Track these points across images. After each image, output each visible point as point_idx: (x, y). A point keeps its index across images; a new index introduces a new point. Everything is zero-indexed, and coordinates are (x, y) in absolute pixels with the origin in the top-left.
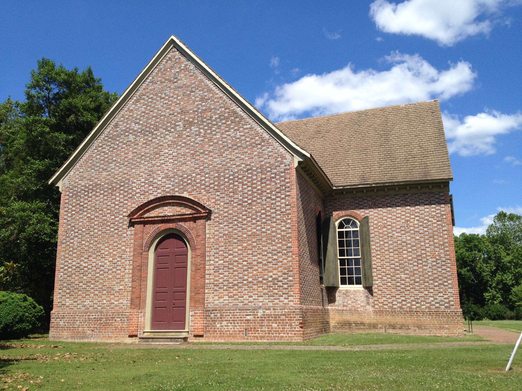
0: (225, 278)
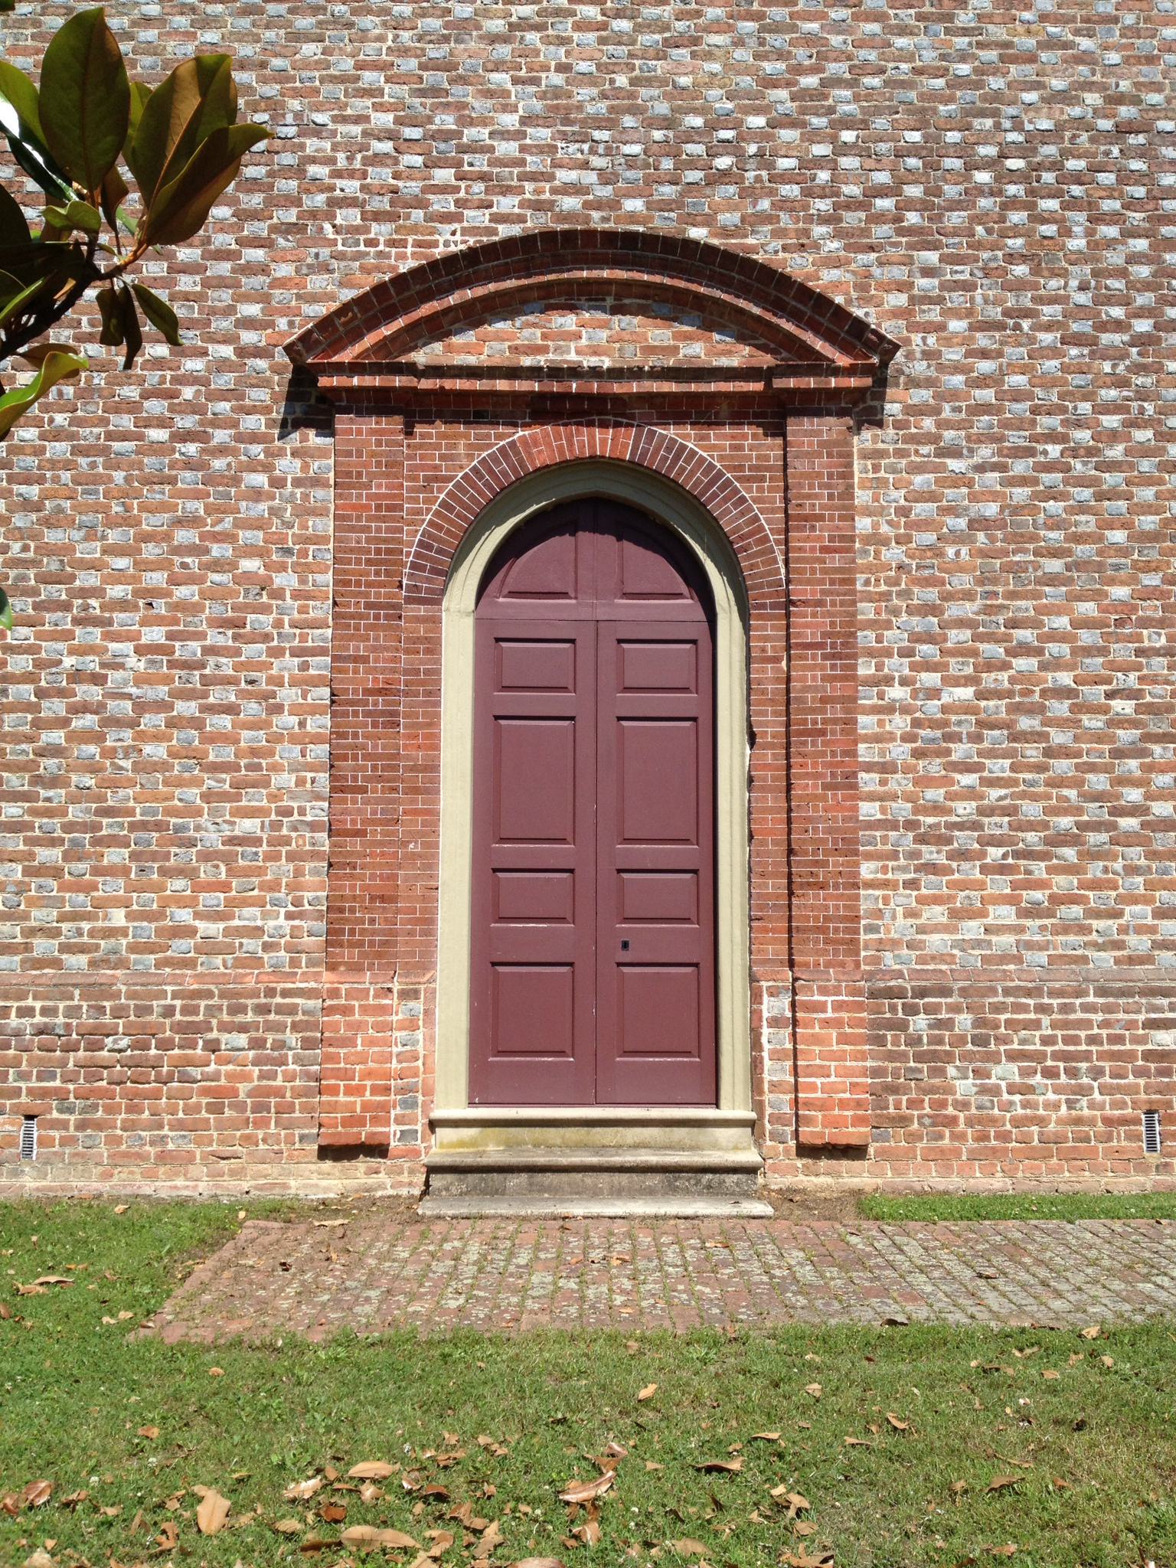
0: (995, 793)
